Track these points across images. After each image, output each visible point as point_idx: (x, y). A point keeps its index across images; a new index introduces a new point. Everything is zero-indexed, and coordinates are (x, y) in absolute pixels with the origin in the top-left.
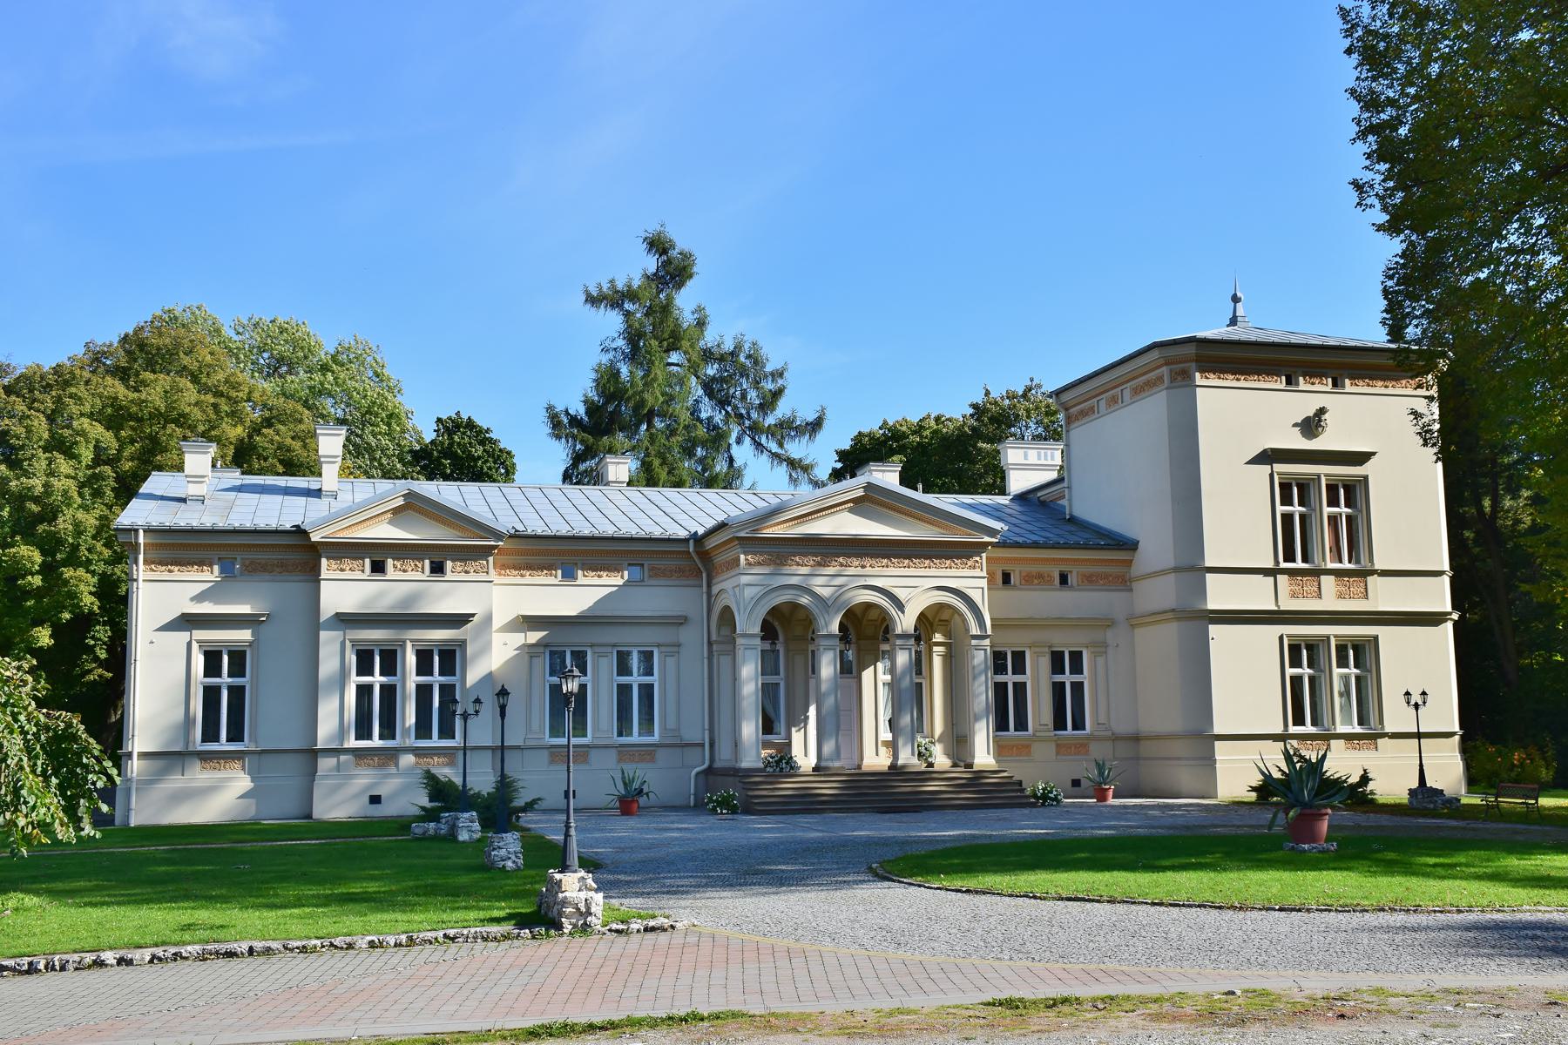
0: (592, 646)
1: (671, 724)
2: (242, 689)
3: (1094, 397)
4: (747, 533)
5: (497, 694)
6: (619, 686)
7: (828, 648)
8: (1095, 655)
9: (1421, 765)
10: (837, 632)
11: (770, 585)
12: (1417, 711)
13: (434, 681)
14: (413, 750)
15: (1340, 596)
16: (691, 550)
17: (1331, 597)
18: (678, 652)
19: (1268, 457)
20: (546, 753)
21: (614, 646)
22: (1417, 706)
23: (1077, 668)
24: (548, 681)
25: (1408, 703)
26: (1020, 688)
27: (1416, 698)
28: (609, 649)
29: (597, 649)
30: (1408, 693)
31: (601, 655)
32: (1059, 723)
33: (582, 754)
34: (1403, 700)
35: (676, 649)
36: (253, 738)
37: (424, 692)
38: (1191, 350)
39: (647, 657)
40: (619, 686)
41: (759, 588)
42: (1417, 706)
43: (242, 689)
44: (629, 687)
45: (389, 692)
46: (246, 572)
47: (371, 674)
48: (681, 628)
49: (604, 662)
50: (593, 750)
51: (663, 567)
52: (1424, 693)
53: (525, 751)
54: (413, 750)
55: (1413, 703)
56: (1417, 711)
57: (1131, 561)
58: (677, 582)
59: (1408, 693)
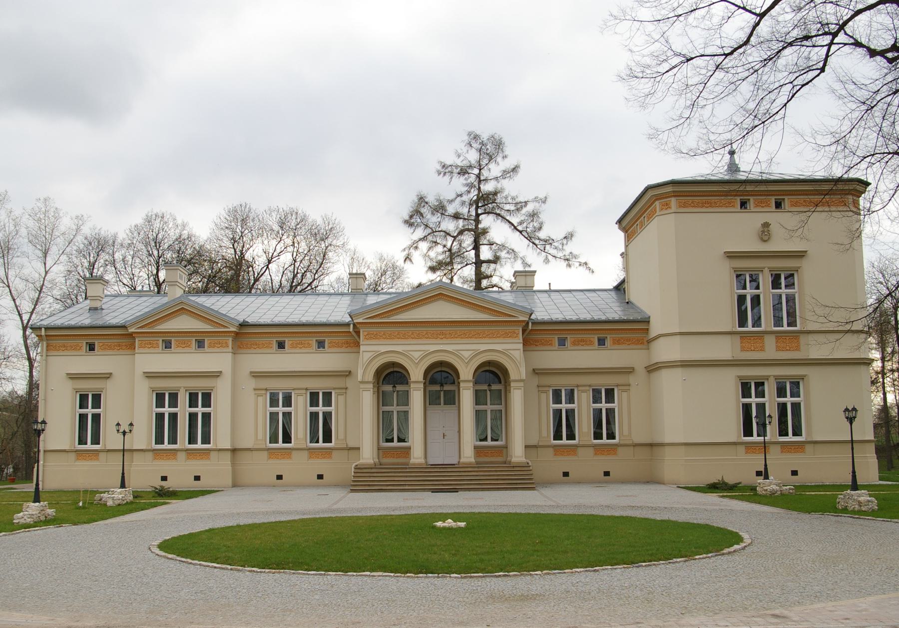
0: (334, 389)
1: (341, 436)
2: (290, 414)
3: (633, 225)
4: (363, 319)
5: (844, 411)
6: (311, 413)
7: (416, 389)
8: (338, 395)
9: (123, 474)
10: (422, 380)
11: (379, 352)
12: (124, 436)
13: (788, 401)
14: (186, 451)
15: (778, 349)
16: (351, 330)
17: (770, 350)
18: (346, 393)
19: (731, 256)
20: (551, 450)
21: (590, 386)
22: (124, 433)
23: (327, 402)
24: (592, 407)
25: (118, 431)
26: (570, 413)
27: (124, 427)
28: (587, 388)
29: (620, 388)
30: (118, 424)
31: (583, 391)
32: (598, 435)
33: (403, 452)
34: (115, 428)
35: (344, 391)
36: (809, 433)
37: (193, 417)
38: (669, 189)
39: (571, 393)
40: (311, 413)
41: (472, 352)
42: (124, 433)
43: (290, 414)
44: (196, 414)
45: (174, 417)
46: (100, 350)
47: (317, 405)
48: (108, 380)
49: (584, 395)
50: (293, 451)
51: (109, 344)
52: (131, 424)
53: (539, 448)
54: (186, 451)
55: (121, 430)
56: (124, 436)
57: (648, 329)
58: (347, 350)
59: (118, 424)
